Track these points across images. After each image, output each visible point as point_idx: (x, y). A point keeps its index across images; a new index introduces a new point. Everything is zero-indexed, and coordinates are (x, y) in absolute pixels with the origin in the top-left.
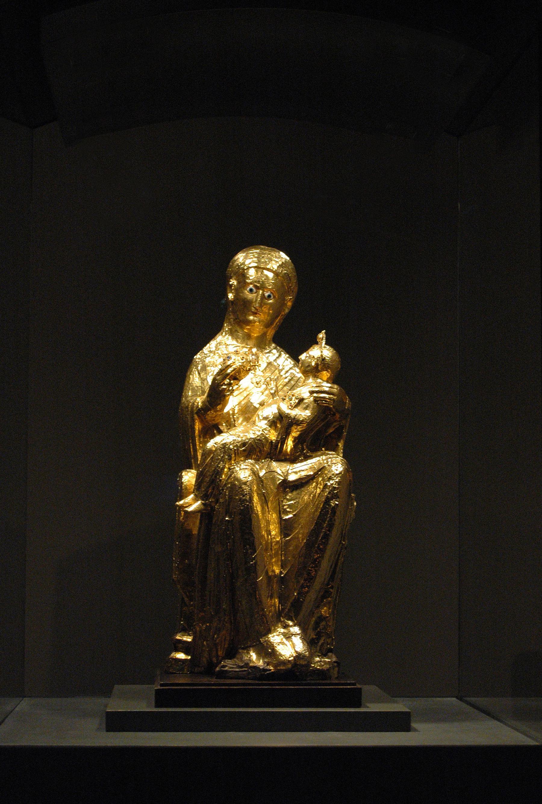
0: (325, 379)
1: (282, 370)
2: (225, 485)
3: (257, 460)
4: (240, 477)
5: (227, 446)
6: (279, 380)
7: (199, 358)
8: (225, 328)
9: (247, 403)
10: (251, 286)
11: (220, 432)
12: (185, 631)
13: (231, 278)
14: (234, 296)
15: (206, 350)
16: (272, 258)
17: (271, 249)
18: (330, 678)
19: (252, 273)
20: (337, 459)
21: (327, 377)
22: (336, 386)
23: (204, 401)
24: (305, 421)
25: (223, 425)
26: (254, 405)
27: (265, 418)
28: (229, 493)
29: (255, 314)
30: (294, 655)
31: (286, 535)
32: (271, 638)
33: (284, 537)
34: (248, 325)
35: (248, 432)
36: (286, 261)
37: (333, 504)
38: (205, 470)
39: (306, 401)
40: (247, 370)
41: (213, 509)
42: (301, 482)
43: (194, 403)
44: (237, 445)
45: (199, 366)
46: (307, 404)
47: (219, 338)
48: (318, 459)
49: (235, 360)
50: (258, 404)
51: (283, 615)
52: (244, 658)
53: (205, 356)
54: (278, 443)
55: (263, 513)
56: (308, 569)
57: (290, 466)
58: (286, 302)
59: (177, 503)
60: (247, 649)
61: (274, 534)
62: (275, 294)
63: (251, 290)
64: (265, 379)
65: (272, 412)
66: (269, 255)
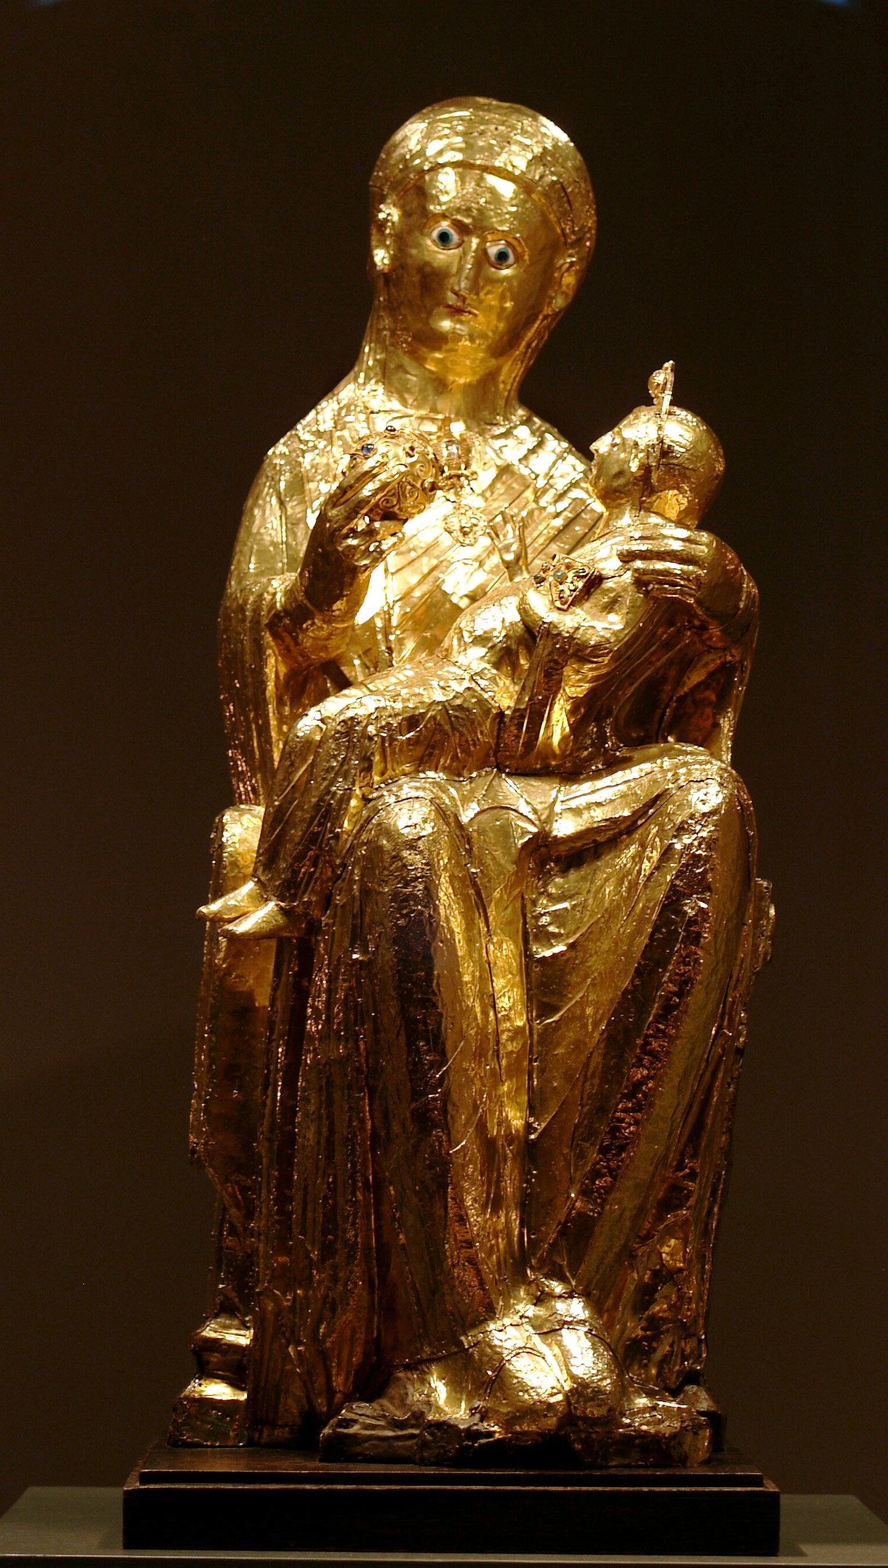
0: (673, 514)
1: (545, 491)
2: (352, 849)
3: (456, 772)
4: (395, 824)
5: (357, 728)
6: (534, 521)
7: (282, 455)
8: (365, 358)
9: (431, 593)
10: (445, 225)
11: (343, 683)
12: (228, 1310)
13: (383, 200)
14: (393, 258)
15: (303, 429)
16: (512, 134)
17: (507, 108)
18: (684, 1460)
19: (447, 182)
20: (709, 766)
21: (677, 508)
22: (705, 537)
23: (291, 590)
24: (606, 648)
25: (354, 666)
26: (455, 599)
27: (481, 640)
28: (362, 876)
29: (456, 312)
30: (567, 1388)
31: (546, 1009)
32: (494, 1332)
33: (538, 1017)
34: (438, 349)
35: (425, 684)
36: (555, 146)
37: (693, 909)
38: (291, 803)
39: (609, 584)
40: (424, 489)
41: (314, 928)
42: (595, 841)
43: (261, 595)
44: (388, 723)
45: (282, 478)
46: (612, 595)
47: (347, 392)
48: (647, 767)
49: (384, 455)
50: (466, 596)
51: (533, 1261)
52: (410, 1398)
53: (302, 446)
54: (523, 717)
55: (470, 941)
56: (613, 1117)
57: (559, 791)
58: (556, 275)
59: (203, 909)
60: (419, 1367)
61: (507, 1006)
62: (519, 249)
63: (444, 238)
64: (491, 517)
65: (503, 621)
66: (503, 125)
